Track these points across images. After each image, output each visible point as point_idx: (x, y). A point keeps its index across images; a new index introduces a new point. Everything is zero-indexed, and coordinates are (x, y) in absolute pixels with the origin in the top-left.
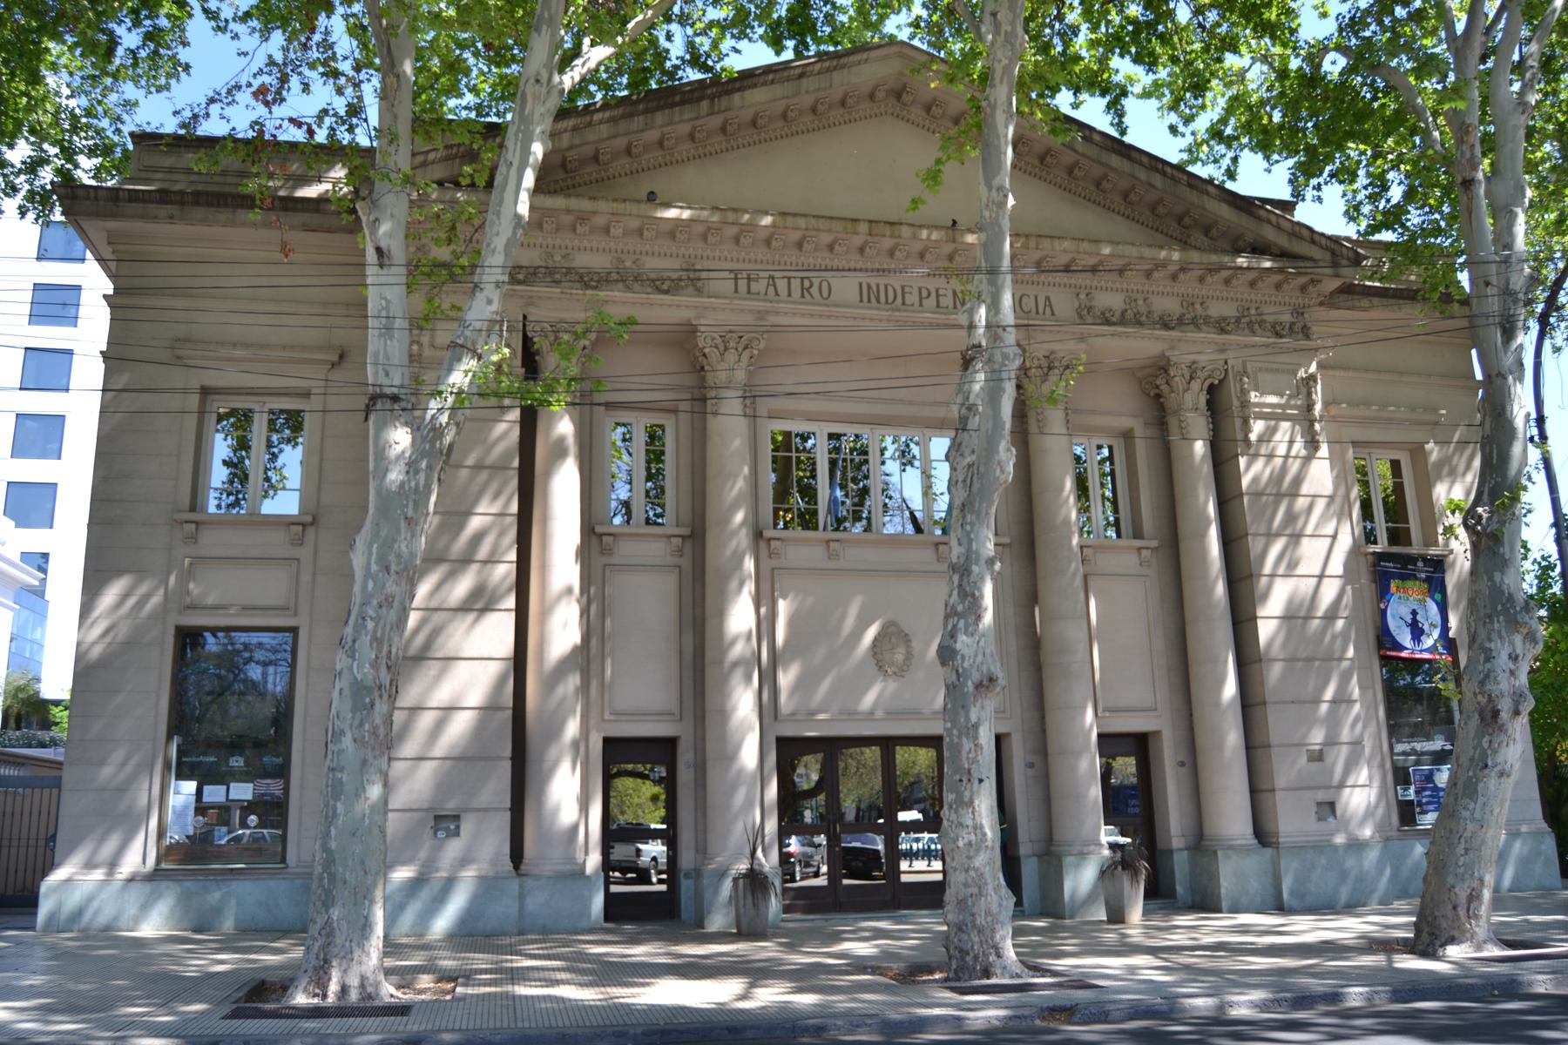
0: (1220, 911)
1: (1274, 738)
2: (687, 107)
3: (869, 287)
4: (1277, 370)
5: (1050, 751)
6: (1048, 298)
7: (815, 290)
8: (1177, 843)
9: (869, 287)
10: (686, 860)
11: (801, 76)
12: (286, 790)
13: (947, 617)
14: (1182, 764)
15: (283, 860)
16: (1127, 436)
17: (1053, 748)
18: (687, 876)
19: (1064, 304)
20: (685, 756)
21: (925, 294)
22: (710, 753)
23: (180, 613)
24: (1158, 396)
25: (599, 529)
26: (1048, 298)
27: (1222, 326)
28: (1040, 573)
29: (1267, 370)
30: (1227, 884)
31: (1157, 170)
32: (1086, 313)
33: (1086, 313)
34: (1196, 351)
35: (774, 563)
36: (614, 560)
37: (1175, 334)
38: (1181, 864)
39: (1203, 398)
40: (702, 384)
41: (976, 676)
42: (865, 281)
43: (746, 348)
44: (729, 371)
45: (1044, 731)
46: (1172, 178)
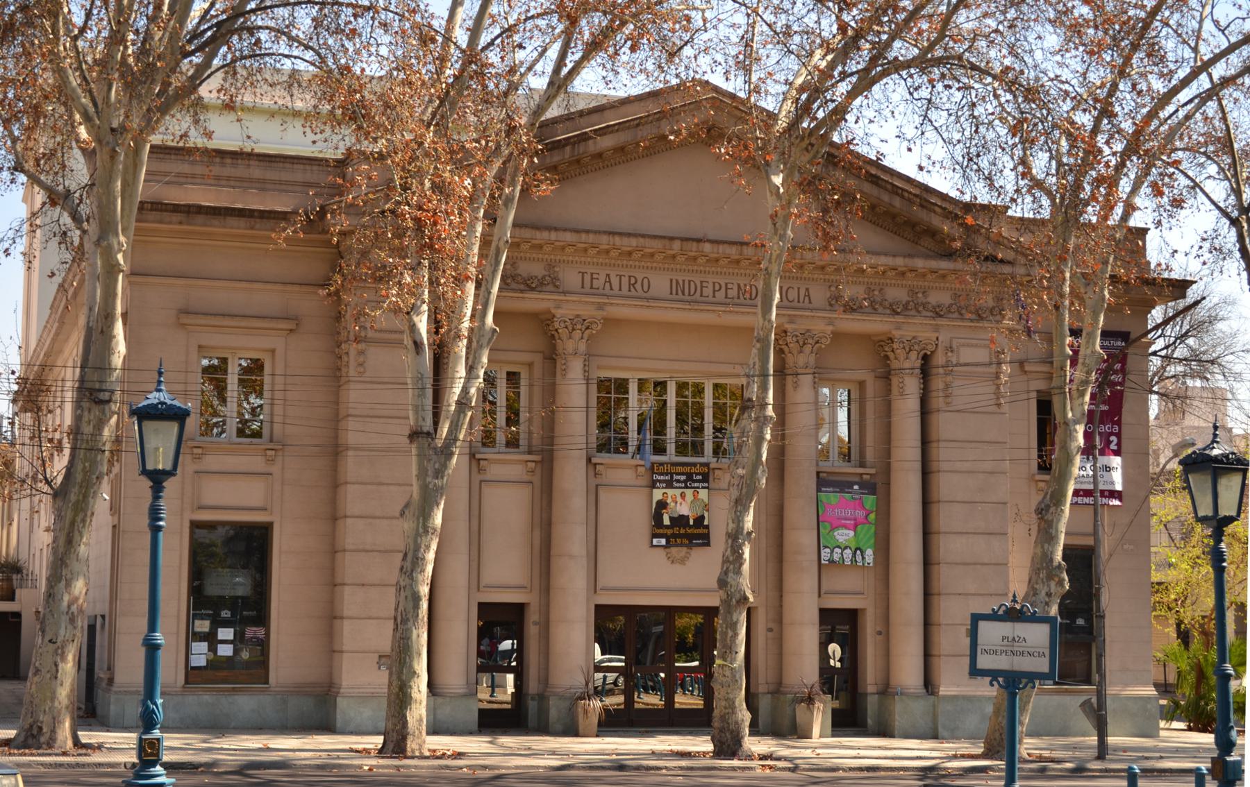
0: (892, 736)
1: (943, 620)
2: (556, 152)
3: (677, 282)
4: (976, 346)
5: (785, 621)
6: (807, 289)
7: (638, 286)
8: (871, 689)
9: (677, 282)
10: (533, 686)
11: (638, 125)
12: (268, 634)
13: (724, 562)
14: (880, 633)
15: (267, 682)
16: (862, 384)
17: (787, 619)
18: (533, 699)
19: (819, 295)
20: (532, 616)
21: (717, 287)
22: (553, 616)
23: (193, 512)
24: (887, 357)
25: (478, 456)
26: (807, 289)
27: (937, 313)
28: (786, 495)
29: (968, 345)
30: (899, 719)
31: (897, 194)
32: (834, 300)
33: (834, 300)
34: (917, 329)
35: (598, 481)
36: (488, 476)
37: (899, 319)
38: (872, 703)
39: (918, 363)
40: (553, 348)
41: (738, 596)
42: (674, 278)
43: (587, 328)
44: (571, 344)
45: (781, 606)
46: (909, 200)
